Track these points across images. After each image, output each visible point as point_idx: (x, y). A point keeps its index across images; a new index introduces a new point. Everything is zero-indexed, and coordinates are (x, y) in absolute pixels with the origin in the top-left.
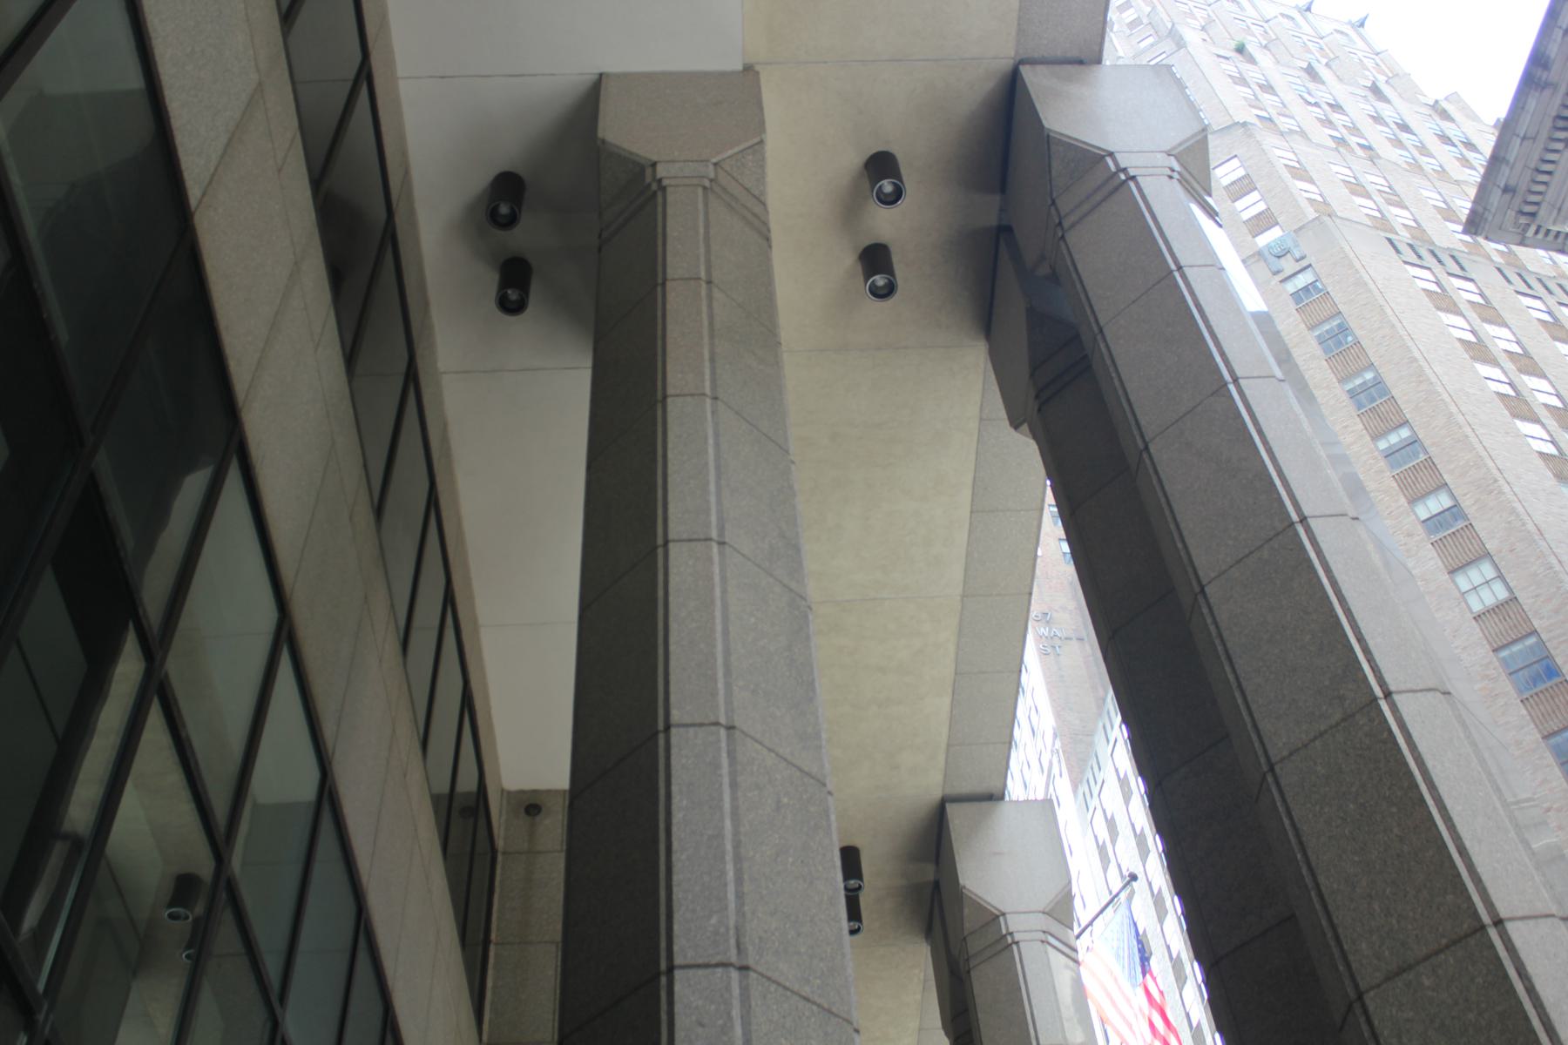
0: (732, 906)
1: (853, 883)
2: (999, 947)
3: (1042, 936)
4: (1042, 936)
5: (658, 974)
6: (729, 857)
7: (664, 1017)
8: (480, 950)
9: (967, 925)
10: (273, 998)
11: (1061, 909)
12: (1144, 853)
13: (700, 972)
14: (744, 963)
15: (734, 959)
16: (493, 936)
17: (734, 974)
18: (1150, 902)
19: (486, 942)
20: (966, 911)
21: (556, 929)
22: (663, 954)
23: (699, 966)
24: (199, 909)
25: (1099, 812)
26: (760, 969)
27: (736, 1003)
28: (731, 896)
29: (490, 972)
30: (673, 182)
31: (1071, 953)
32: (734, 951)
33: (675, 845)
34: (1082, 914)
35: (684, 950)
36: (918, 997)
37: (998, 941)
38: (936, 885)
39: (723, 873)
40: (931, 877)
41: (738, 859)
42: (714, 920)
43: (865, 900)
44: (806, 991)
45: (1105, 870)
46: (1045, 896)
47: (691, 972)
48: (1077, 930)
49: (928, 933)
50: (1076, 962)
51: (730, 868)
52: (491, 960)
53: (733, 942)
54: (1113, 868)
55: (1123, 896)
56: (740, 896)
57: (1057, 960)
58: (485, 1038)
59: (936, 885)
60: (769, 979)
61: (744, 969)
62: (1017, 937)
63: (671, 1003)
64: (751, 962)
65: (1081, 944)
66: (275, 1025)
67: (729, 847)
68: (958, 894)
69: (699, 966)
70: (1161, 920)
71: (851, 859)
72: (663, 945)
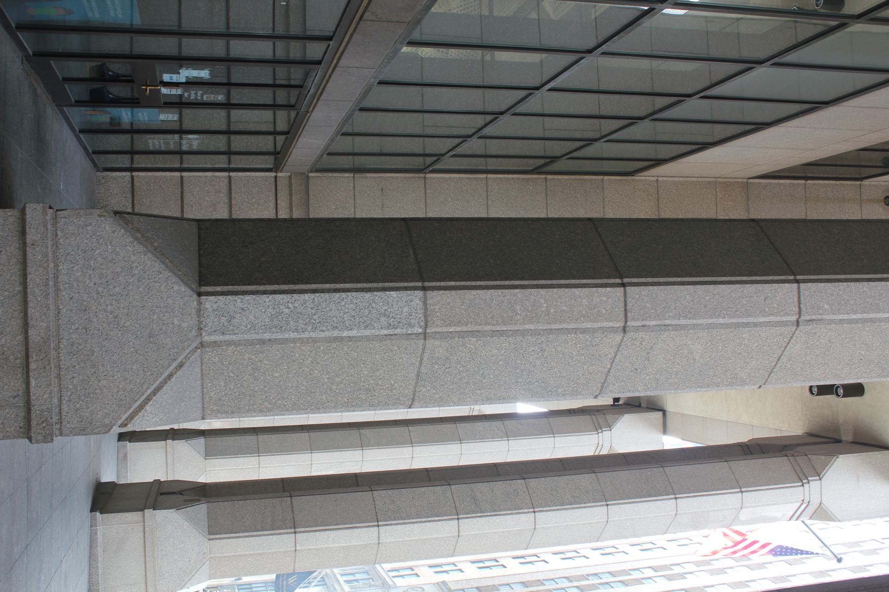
0: (835, 317)
1: (841, 391)
2: (800, 475)
3: (806, 501)
4: (806, 501)
5: (795, 275)
6: (865, 316)
7: (770, 278)
8: (802, 175)
9: (814, 457)
10: (775, 60)
11: (822, 513)
12: (853, 569)
13: (796, 298)
14: (801, 324)
15: (803, 318)
16: (809, 182)
17: (794, 318)
18: (743, 579)
19: (806, 178)
20: (823, 457)
21: (814, 215)
22: (806, 277)
23: (799, 297)
24: (822, 11)
25: (881, 546)
26: (797, 332)
27: (778, 319)
28: (841, 317)
29: (788, 181)
30: (807, 492)
31: (796, 516)
32: (808, 318)
33: (528, 291)
34: (817, 525)
35: (808, 289)
36: (771, 426)
37: (804, 474)
38: (839, 441)
39: (855, 312)
40: (843, 438)
41: (864, 321)
42: (826, 306)
43: (831, 398)
44: (784, 359)
45: (844, 544)
46: (831, 504)
47: (796, 293)
48: (808, 522)
49: (810, 435)
50: (790, 519)
51: (859, 316)
52: (795, 182)
53: (814, 317)
54: (846, 550)
55: (829, 553)
56: (841, 321)
57: (791, 508)
58: (751, 181)
59: (839, 441)
60: (791, 338)
61: (624, 330)
62: (806, 486)
63: (778, 282)
64: (801, 328)
65: (799, 522)
66: (760, 62)
67: (871, 316)
68: (835, 454)
69: (799, 297)
70: (811, 573)
71: (856, 390)
72: (812, 277)
